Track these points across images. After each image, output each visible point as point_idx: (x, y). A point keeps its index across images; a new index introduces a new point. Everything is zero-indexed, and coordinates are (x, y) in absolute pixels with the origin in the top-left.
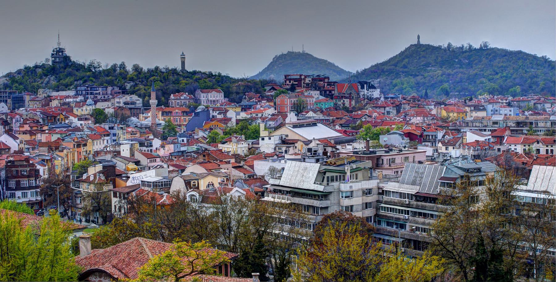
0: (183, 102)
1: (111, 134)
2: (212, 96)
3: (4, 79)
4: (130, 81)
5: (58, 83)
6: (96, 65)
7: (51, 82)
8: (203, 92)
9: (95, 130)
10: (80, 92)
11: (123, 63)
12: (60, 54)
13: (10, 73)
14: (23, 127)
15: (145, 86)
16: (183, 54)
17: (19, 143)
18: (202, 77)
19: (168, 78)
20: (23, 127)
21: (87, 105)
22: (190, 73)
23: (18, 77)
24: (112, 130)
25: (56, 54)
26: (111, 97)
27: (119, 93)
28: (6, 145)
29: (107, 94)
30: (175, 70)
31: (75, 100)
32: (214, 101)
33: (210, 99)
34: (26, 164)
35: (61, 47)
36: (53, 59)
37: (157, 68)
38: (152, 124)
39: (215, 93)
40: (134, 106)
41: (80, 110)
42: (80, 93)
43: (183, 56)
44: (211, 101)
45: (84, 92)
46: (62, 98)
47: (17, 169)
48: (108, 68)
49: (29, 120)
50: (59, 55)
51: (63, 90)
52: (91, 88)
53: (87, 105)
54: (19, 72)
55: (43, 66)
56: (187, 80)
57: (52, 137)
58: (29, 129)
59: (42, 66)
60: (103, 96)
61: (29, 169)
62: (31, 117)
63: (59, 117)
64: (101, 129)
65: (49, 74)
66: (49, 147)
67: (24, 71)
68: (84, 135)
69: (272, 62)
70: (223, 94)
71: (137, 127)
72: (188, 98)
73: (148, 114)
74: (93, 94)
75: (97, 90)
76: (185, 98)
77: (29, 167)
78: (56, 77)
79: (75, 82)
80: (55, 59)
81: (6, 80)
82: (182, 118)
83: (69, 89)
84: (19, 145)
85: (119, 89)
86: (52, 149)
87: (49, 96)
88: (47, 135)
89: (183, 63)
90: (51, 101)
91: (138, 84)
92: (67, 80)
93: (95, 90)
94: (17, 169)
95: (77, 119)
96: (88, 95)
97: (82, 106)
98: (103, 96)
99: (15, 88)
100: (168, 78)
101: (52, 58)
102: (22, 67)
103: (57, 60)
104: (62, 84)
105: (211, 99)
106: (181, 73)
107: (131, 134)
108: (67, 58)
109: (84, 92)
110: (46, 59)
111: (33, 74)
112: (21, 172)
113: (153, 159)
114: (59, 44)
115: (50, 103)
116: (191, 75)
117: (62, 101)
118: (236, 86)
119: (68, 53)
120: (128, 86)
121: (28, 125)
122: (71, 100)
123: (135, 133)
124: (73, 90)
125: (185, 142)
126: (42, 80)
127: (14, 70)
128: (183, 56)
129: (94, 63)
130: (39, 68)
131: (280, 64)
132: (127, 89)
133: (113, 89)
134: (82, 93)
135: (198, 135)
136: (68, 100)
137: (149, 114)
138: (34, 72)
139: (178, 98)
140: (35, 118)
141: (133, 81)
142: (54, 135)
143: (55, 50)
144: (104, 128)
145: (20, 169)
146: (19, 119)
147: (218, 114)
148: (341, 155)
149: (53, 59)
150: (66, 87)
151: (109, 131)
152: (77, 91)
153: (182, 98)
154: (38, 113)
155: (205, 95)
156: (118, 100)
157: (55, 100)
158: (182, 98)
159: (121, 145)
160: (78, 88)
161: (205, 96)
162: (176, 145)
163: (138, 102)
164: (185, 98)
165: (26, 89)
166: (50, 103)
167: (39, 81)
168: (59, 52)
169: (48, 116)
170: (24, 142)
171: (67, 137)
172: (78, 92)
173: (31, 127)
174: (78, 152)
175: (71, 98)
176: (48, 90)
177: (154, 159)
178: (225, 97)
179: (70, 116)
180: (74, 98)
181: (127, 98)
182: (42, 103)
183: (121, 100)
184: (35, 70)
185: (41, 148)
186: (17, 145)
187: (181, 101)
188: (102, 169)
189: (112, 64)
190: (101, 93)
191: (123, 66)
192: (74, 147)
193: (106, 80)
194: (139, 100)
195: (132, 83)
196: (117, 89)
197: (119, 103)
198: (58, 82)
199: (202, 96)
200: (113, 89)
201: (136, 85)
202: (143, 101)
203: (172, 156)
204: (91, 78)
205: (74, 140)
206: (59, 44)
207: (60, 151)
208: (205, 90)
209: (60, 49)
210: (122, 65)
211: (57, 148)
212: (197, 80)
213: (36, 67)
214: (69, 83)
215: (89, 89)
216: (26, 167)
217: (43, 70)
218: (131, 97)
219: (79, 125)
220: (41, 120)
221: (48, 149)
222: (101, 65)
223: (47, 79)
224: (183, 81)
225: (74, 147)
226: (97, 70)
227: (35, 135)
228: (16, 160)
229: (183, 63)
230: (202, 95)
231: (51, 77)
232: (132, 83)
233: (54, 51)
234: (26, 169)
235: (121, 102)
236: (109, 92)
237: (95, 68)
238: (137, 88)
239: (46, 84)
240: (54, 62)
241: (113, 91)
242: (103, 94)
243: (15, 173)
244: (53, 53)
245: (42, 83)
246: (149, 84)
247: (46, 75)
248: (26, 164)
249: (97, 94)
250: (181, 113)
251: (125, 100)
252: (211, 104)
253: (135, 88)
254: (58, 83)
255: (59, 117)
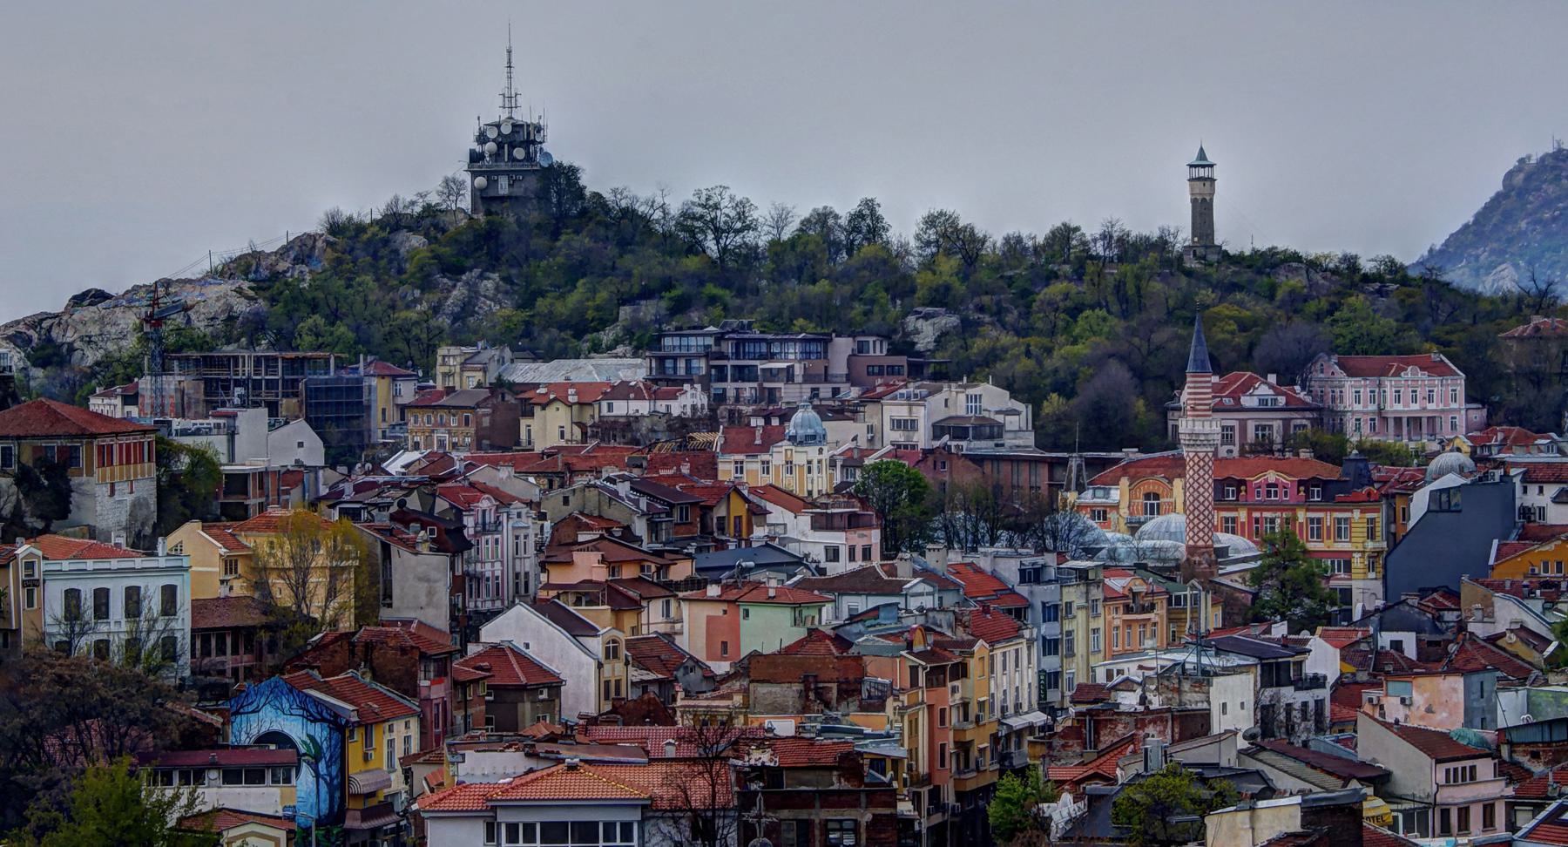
0: (1251, 426)
1: (1030, 606)
2: (1406, 394)
3: (227, 287)
4: (932, 303)
5: (525, 314)
6: (727, 211)
7: (485, 305)
8: (1351, 373)
9: (957, 588)
10: (682, 364)
11: (870, 205)
12: (519, 153)
13: (256, 255)
14: (570, 563)
15: (1018, 333)
16: (1202, 162)
17: (601, 655)
18: (1312, 284)
19: (1138, 289)
20: (570, 563)
21: (793, 439)
22: (1238, 260)
23: (304, 277)
24: (1037, 588)
25: (497, 156)
26: (854, 393)
27: (893, 370)
28: (540, 667)
29: (826, 378)
30: (1162, 244)
31: (661, 406)
32: (1415, 421)
33: (1393, 408)
34: (845, 785)
35: (522, 116)
36: (481, 181)
37: (1063, 235)
38: (1192, 550)
39: (1421, 375)
40: (991, 443)
41: (753, 466)
42: (682, 372)
43: (1202, 172)
44: (1398, 420)
45: (701, 365)
46: (587, 397)
47: (803, 815)
48: (786, 235)
49: (588, 528)
50: (513, 159)
51: (563, 354)
52: (739, 343)
53: (793, 439)
54: (302, 250)
55: (429, 220)
56: (1241, 304)
57: (745, 625)
58: (601, 575)
59: (421, 217)
60: (807, 388)
61: (868, 817)
62: (591, 507)
63: (721, 511)
64: (976, 578)
65: (469, 263)
66: (805, 681)
67: (328, 243)
68: (940, 617)
69: (1498, 198)
70: (1459, 383)
71: (1144, 567)
72: (1282, 400)
73: (1107, 495)
74: (755, 379)
75: (770, 356)
76: (1263, 401)
77: (870, 804)
78: (507, 280)
79: (625, 312)
80: (492, 183)
81: (239, 291)
82: (1302, 516)
83: (596, 348)
84: (600, 666)
85: (891, 352)
86: (820, 694)
87: (500, 387)
88: (717, 610)
89: (1203, 211)
90: (530, 414)
91: (979, 323)
92: (574, 298)
93: (762, 357)
94: (803, 815)
95: (805, 520)
96: (723, 379)
97: (765, 448)
98: (807, 388)
99: (308, 339)
100: (1138, 289)
101: (475, 174)
102: (314, 224)
103: (503, 187)
104: (550, 320)
105: (1399, 407)
106: (1191, 263)
107: (1128, 610)
108: (562, 179)
109: (701, 365)
110: (447, 181)
111: (383, 263)
112: (826, 830)
113: (1459, 765)
114: (510, 100)
115: (524, 422)
116: (1247, 275)
117: (588, 412)
118: (1521, 339)
119: (558, 148)
120: (925, 333)
121: (597, 556)
122: (643, 407)
123: (1147, 601)
124: (620, 349)
125: (1410, 650)
126: (433, 297)
127: (271, 240)
128: (1202, 172)
129: (716, 207)
130: (410, 229)
131: (1548, 203)
132: (920, 347)
133: (861, 348)
134: (688, 368)
135: (1488, 615)
136: (621, 408)
137: (1115, 495)
138: (383, 252)
139: (1228, 402)
140: (612, 512)
141: (951, 308)
142: (753, 611)
143: (492, 134)
144: (994, 576)
145: (819, 815)
146: (490, 518)
147: (1557, 500)
148: (498, 573)
149: (481, 181)
150: (579, 335)
151: (1023, 590)
152: (661, 360)
153: (1247, 401)
154: (623, 489)
155: (1364, 386)
156: (902, 412)
157: (551, 410)
158: (1247, 401)
159: (1216, 680)
160: (668, 341)
161: (1365, 393)
162: (1476, 678)
163: (1012, 423)
164: (1263, 401)
165: (362, 343)
166: (524, 422)
167: (416, 301)
168: (512, 146)
169: (672, 506)
170: (623, 652)
171: (859, 627)
172: (669, 363)
173: (613, 566)
174: (930, 707)
175: (639, 397)
176: (494, 352)
177: (1468, 763)
178: (1469, 399)
179: (769, 506)
180: (655, 396)
181: (954, 400)
182: (478, 424)
183: (920, 413)
184: (386, 242)
185: (763, 689)
186: (593, 664)
187: (1243, 423)
188: (1295, 826)
189: (805, 212)
190: (798, 370)
191: (867, 222)
192: (914, 683)
193: (804, 302)
194: (1018, 413)
195: (949, 321)
196: (877, 351)
197: (907, 425)
198: (519, 307)
199: (1349, 394)
200: (861, 348)
201: (968, 328)
202: (1036, 416)
203: (1511, 744)
204: (711, 289)
205: (910, 646)
206: (510, 100)
207: (863, 708)
208: (1357, 361)
209: (517, 127)
210: (859, 216)
211: (849, 690)
212: (1296, 302)
213: (394, 222)
214: (590, 314)
215: (728, 348)
216: (854, 805)
217: (432, 240)
218: (977, 398)
219: (818, 554)
220: (640, 528)
221: (804, 695)
222: (755, 214)
223: (459, 292)
224: (1223, 309)
225: (914, 683)
226: (733, 241)
227: (636, 606)
228: (789, 761)
229: (1203, 211)
230: (1350, 386)
231: (481, 277)
232: (949, 321)
233: (482, 138)
234: (848, 814)
235: (921, 425)
236: (840, 367)
237: (718, 232)
238: (979, 345)
239: (456, 318)
240: (484, 198)
241: (862, 363)
242: (808, 378)
243: (793, 835)
244: (478, 149)
245: (436, 310)
246: (1039, 325)
247: (454, 270)
248: (845, 785)
249: (771, 375)
250: (1292, 490)
251: (941, 414)
252: (1398, 434)
253: (966, 348)
254: (525, 314)
255: (721, 511)
